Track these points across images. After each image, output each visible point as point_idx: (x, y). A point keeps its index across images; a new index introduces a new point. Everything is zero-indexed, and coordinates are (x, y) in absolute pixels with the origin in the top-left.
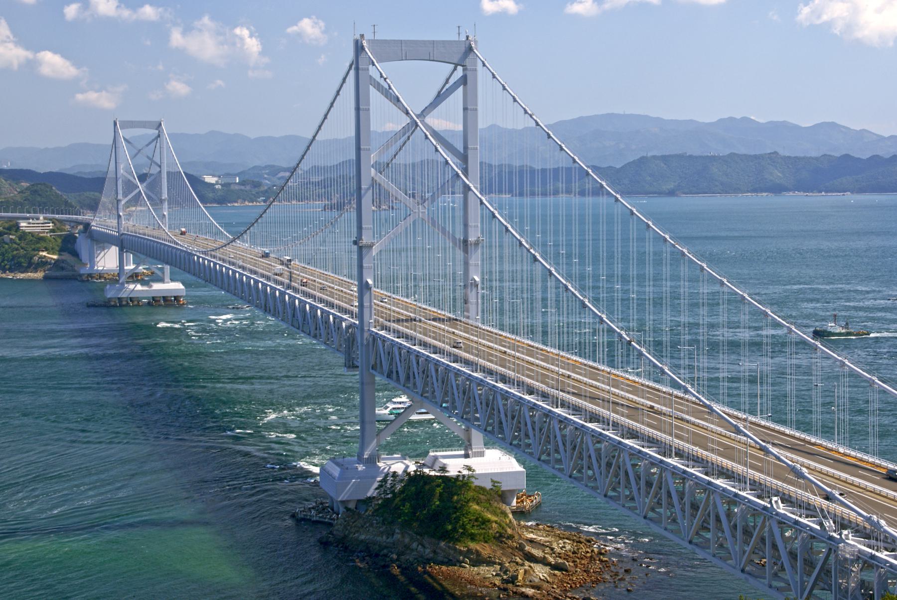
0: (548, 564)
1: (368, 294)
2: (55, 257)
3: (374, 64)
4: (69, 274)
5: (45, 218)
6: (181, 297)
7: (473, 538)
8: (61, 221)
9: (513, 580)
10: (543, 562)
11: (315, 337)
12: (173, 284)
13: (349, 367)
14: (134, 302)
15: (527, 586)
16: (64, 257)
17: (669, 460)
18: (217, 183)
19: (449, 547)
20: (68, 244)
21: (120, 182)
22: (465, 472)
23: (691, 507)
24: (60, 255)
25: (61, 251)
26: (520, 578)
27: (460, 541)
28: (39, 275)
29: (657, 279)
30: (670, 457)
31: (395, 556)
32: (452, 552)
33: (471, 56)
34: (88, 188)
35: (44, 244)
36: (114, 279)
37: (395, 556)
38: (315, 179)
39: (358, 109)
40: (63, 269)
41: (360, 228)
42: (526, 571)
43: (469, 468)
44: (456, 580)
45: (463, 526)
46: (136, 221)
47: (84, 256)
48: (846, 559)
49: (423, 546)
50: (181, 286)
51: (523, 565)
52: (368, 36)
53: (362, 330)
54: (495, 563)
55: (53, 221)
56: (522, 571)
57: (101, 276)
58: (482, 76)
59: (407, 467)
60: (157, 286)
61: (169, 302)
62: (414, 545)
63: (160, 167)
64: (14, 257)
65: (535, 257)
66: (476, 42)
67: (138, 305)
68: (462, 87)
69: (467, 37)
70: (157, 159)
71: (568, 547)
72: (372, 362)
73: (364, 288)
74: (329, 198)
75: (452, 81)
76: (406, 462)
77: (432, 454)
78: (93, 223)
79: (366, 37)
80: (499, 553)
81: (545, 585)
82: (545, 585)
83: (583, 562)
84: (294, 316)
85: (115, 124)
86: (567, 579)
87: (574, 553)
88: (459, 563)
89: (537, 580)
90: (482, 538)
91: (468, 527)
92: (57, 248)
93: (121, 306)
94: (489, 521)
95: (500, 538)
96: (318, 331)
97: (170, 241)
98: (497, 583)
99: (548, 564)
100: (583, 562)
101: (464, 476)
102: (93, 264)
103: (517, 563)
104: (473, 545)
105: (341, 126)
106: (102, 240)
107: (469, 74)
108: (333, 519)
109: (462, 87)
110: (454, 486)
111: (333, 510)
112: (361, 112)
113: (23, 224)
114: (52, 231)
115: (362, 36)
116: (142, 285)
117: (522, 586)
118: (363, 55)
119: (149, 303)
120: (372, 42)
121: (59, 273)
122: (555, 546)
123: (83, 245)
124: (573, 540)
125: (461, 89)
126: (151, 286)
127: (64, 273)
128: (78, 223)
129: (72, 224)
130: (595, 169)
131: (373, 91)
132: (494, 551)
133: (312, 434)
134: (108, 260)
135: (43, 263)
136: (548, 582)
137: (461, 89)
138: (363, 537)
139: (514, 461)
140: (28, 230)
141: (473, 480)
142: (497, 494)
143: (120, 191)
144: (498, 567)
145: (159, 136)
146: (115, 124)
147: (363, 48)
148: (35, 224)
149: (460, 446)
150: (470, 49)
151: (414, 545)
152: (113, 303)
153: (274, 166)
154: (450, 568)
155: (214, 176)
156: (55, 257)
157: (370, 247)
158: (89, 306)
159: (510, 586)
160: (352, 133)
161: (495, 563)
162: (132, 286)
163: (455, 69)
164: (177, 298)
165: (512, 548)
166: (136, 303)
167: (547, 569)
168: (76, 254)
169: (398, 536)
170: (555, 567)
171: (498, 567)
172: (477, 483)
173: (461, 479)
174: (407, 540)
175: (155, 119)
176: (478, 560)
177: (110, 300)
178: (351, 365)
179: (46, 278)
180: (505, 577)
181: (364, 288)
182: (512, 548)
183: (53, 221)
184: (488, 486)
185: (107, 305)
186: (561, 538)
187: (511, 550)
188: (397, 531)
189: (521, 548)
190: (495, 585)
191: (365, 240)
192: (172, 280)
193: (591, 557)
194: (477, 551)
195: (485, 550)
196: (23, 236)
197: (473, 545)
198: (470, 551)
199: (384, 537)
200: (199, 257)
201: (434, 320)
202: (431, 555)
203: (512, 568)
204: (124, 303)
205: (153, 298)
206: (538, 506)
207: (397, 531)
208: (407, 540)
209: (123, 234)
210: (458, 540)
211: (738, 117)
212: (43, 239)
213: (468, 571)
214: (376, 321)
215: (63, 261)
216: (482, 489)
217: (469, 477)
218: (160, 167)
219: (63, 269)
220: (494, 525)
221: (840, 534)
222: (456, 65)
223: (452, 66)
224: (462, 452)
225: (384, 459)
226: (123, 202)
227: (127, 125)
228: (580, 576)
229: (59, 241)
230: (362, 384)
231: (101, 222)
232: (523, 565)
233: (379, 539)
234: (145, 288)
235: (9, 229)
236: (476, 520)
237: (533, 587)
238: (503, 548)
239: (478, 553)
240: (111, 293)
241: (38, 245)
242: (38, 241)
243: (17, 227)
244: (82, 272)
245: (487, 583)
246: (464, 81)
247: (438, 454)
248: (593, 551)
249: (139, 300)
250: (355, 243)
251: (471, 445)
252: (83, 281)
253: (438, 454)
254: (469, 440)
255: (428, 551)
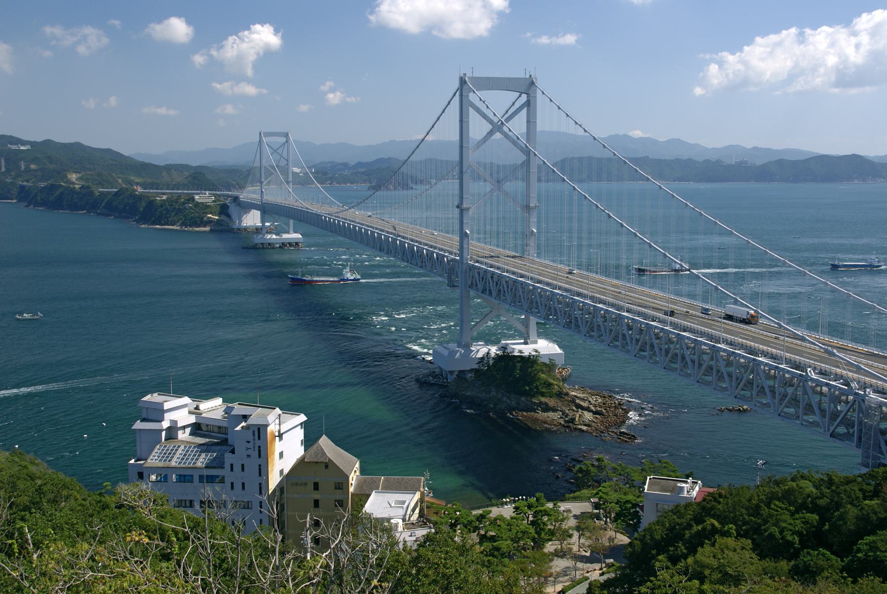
0: (592, 411)
4: (225, 228)
7: (543, 394)
8: (219, 196)
9: (572, 420)
10: (588, 409)
11: (421, 267)
14: (270, 245)
20: (224, 210)
21: (263, 170)
22: (534, 353)
23: (460, 371)
25: (220, 214)
28: (207, 229)
31: (492, 405)
33: (533, 88)
34: (241, 175)
35: (209, 210)
36: (258, 230)
37: (492, 405)
38: (361, 170)
39: (461, 121)
40: (222, 225)
41: (461, 197)
43: (536, 351)
44: (536, 420)
45: (537, 387)
46: (275, 195)
48: (870, 407)
52: (469, 74)
55: (215, 195)
57: (245, 229)
58: (541, 102)
60: (285, 236)
64: (192, 218)
70: (285, 155)
71: (600, 400)
73: (463, 236)
74: (370, 182)
75: (517, 105)
80: (560, 404)
81: (593, 424)
82: (593, 424)
88: (534, 411)
93: (263, 248)
95: (560, 395)
98: (562, 423)
99: (592, 411)
104: (543, 399)
105: (449, 131)
106: (247, 207)
107: (531, 99)
110: (529, 362)
113: (197, 197)
114: (214, 201)
118: (465, 87)
120: (471, 78)
121: (220, 228)
122: (590, 399)
123: (233, 210)
125: (525, 110)
130: (631, 160)
133: (417, 329)
134: (252, 219)
135: (210, 222)
137: (525, 110)
138: (469, 394)
140: (200, 201)
142: (550, 366)
143: (263, 176)
147: (465, 82)
148: (204, 197)
149: (520, 337)
150: (533, 83)
151: (505, 399)
157: (468, 209)
159: (571, 424)
160: (458, 138)
163: (520, 96)
164: (297, 244)
168: (229, 216)
169: (493, 393)
170: (595, 413)
172: (541, 360)
174: (500, 396)
176: (547, 408)
177: (256, 244)
178: (452, 285)
179: (211, 231)
181: (463, 236)
183: (215, 195)
185: (255, 247)
189: (573, 401)
191: (465, 206)
192: (295, 232)
195: (551, 402)
196: (197, 204)
197: (543, 399)
198: (541, 403)
200: (325, 217)
203: (571, 414)
206: (570, 375)
208: (500, 396)
210: (533, 396)
212: (209, 206)
213: (541, 415)
216: (545, 364)
217: (537, 356)
219: (222, 225)
221: (865, 392)
227: (268, 134)
231: (246, 195)
235: (188, 200)
236: (545, 383)
237: (585, 425)
239: (546, 404)
242: (205, 207)
243: (193, 199)
246: (528, 104)
250: (458, 207)
254: (528, 333)
255: (513, 403)
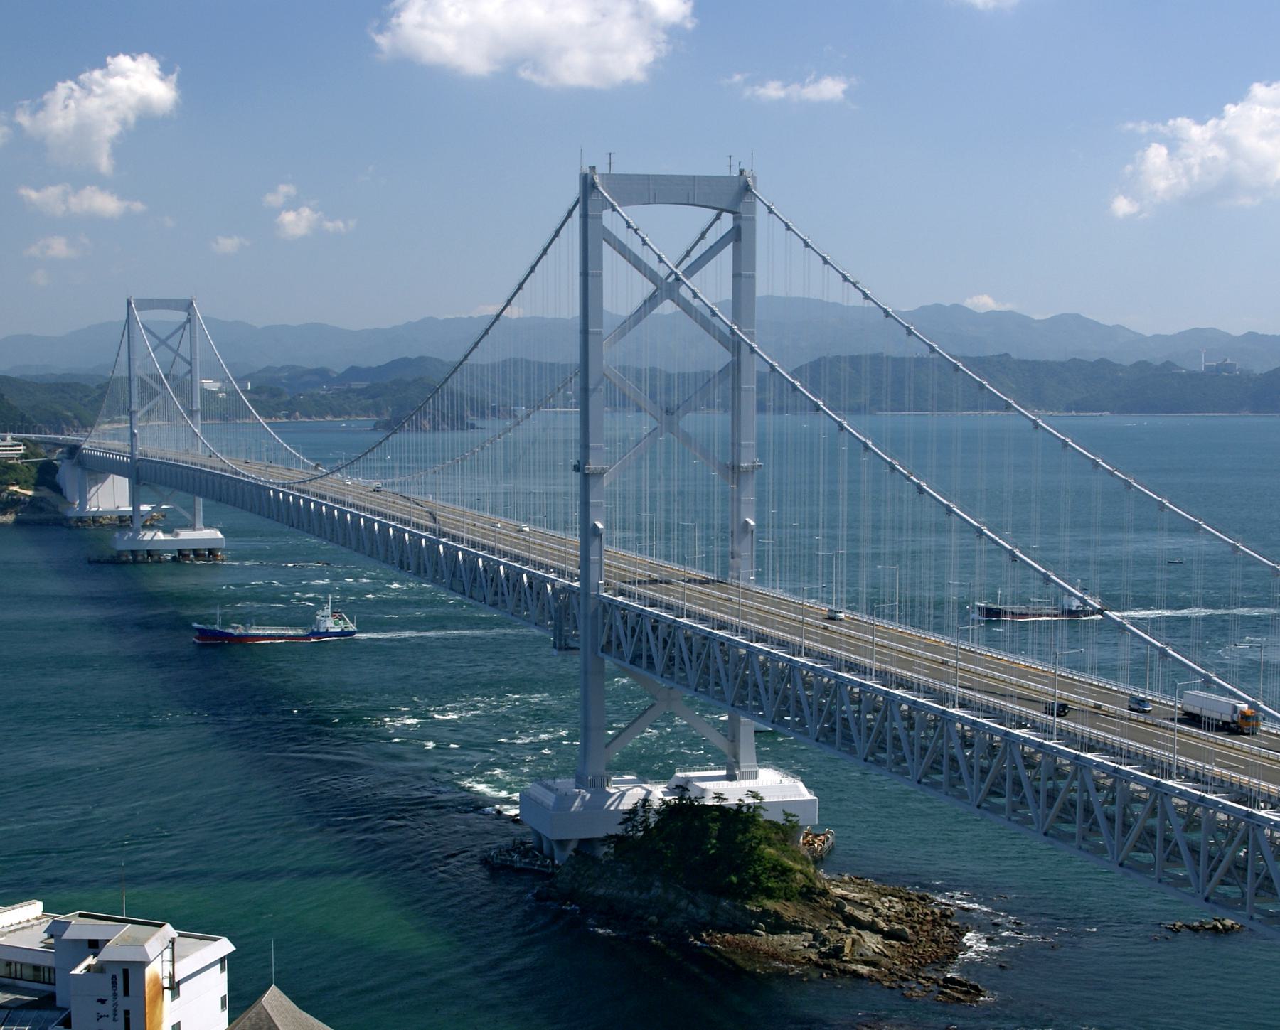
1: (596, 543)
2: (30, 493)
3: (614, 209)
5: (13, 439)
7: (770, 893)
8: (36, 443)
9: (837, 952)
10: (872, 928)
11: (494, 605)
13: (560, 649)
15: (857, 962)
17: (1170, 782)
18: (220, 391)
19: (735, 907)
20: (46, 475)
21: (135, 384)
22: (749, 800)
24: (36, 490)
25: (36, 486)
26: (847, 950)
27: (750, 899)
28: (9, 518)
30: (1171, 778)
31: (654, 918)
32: (739, 913)
34: (83, 398)
35: (13, 475)
36: (123, 522)
37: (654, 918)
38: (357, 385)
39: (585, 274)
40: (41, 509)
42: (854, 941)
44: (754, 952)
45: (756, 877)
47: (70, 489)
49: (697, 907)
50: (220, 536)
51: (848, 932)
52: (602, 169)
53: (587, 594)
54: (804, 929)
55: (25, 442)
56: (849, 941)
57: (95, 519)
58: (765, 230)
59: (649, 792)
60: (185, 534)
62: (683, 903)
63: (190, 364)
65: (919, 487)
66: (754, 178)
67: (159, 562)
68: (731, 246)
69: (741, 172)
71: (899, 907)
72: (604, 641)
73: (589, 534)
75: (712, 238)
76: (648, 786)
77: (680, 775)
79: (598, 170)
80: (808, 915)
81: (884, 961)
82: (884, 961)
83: (925, 928)
85: (129, 303)
86: (910, 952)
87: (908, 915)
88: (750, 930)
89: (870, 953)
90: (782, 894)
91: (763, 878)
92: (32, 481)
93: (135, 562)
94: (791, 870)
96: (499, 598)
98: (814, 957)
100: (925, 928)
101: (748, 806)
102: (84, 502)
103: (839, 930)
104: (770, 905)
105: (556, 298)
106: (98, 469)
107: (744, 225)
108: (547, 866)
109: (731, 246)
110: (738, 820)
111: (541, 851)
112: (590, 278)
114: (24, 456)
115: (593, 169)
116: (165, 532)
117: (850, 962)
119: (174, 559)
120: (608, 178)
121: (35, 517)
122: (877, 905)
123: (67, 475)
124: (901, 898)
125: (729, 250)
126: (177, 534)
127: (43, 516)
128: (57, 444)
129: (49, 447)
131: (606, 248)
132: (801, 913)
133: (483, 746)
134: (111, 497)
136: (886, 956)
137: (729, 250)
138: (601, 891)
139: (801, 785)
141: (762, 812)
142: (786, 830)
143: (135, 400)
144: (811, 936)
145: (189, 321)
146: (129, 303)
147: (594, 186)
149: (719, 763)
150: (747, 188)
151: (683, 903)
152: (124, 559)
153: (294, 367)
154: (738, 936)
155: (216, 381)
156: (30, 493)
157: (600, 474)
158: (90, 562)
159: (833, 961)
160: (576, 311)
161: (804, 929)
163: (718, 217)
164: (212, 552)
165: (827, 909)
167: (879, 937)
168: (58, 489)
169: (657, 891)
170: (888, 935)
171: (811, 936)
172: (767, 816)
173: (744, 809)
174: (672, 897)
175: (185, 296)
176: (778, 925)
177: (120, 553)
178: (563, 645)
179: (18, 523)
180: (823, 949)
181: (589, 534)
182: (827, 909)
184: (780, 819)
185: (117, 561)
186: (885, 895)
187: (824, 912)
188: (657, 883)
189: (838, 909)
190: (810, 959)
191: (593, 466)
193: (934, 921)
194: (776, 912)
195: (789, 911)
197: (770, 905)
198: (766, 912)
199: (636, 893)
201: (689, 581)
202: (708, 918)
203: (833, 937)
204: (140, 558)
205: (180, 551)
206: (831, 850)
207: (657, 883)
210: (748, 898)
211: (947, 304)
213: (766, 940)
214: (607, 583)
215: (42, 499)
216: (774, 825)
217: (756, 807)
218: (190, 364)
219: (41, 509)
220: (799, 876)
222: (721, 211)
223: (715, 212)
224: (724, 772)
225: (615, 782)
226: (139, 415)
227: (146, 304)
228: (928, 949)
229: (34, 470)
230: (586, 673)
231: (102, 440)
232: (848, 932)
233: (627, 894)
236: (774, 868)
237: (866, 963)
238: (814, 909)
239: (777, 915)
240: (123, 542)
241: (6, 477)
244: (70, 514)
245: (798, 958)
246: (736, 235)
247: (692, 774)
248: (933, 912)
249: (159, 553)
250: (577, 468)
251: (738, 762)
252: (70, 527)
253: (692, 774)
254: (736, 756)
255: (702, 912)
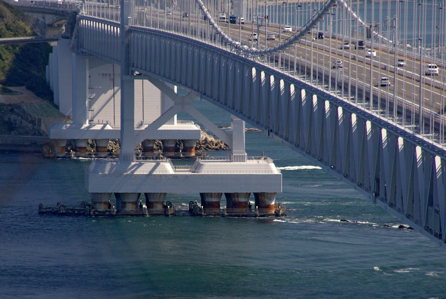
6: (271, 195)
12: (254, 162)
14: (153, 205)
16: (14, 99)
29: (301, 12)
47: (64, 96)
60: (211, 167)
61: (242, 207)
78: (84, 12)
84: (431, 203)
97: (213, 38)
123: (61, 68)
126: (199, 166)
152: (102, 208)
162: (146, 168)
166: (159, 208)
192: (254, 153)
204: (130, 208)
209: (131, 30)
234: (184, 171)
240: (103, 178)
244: (53, 134)
